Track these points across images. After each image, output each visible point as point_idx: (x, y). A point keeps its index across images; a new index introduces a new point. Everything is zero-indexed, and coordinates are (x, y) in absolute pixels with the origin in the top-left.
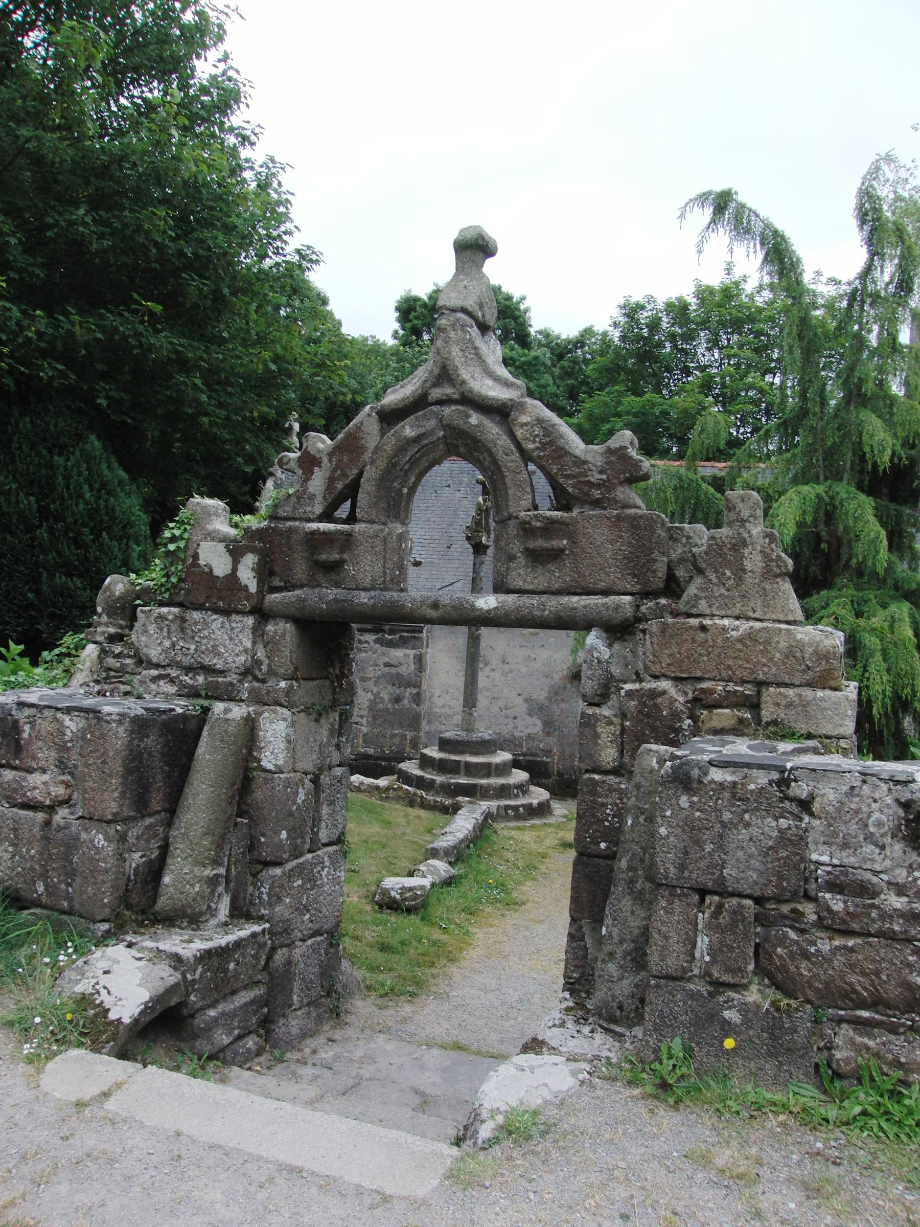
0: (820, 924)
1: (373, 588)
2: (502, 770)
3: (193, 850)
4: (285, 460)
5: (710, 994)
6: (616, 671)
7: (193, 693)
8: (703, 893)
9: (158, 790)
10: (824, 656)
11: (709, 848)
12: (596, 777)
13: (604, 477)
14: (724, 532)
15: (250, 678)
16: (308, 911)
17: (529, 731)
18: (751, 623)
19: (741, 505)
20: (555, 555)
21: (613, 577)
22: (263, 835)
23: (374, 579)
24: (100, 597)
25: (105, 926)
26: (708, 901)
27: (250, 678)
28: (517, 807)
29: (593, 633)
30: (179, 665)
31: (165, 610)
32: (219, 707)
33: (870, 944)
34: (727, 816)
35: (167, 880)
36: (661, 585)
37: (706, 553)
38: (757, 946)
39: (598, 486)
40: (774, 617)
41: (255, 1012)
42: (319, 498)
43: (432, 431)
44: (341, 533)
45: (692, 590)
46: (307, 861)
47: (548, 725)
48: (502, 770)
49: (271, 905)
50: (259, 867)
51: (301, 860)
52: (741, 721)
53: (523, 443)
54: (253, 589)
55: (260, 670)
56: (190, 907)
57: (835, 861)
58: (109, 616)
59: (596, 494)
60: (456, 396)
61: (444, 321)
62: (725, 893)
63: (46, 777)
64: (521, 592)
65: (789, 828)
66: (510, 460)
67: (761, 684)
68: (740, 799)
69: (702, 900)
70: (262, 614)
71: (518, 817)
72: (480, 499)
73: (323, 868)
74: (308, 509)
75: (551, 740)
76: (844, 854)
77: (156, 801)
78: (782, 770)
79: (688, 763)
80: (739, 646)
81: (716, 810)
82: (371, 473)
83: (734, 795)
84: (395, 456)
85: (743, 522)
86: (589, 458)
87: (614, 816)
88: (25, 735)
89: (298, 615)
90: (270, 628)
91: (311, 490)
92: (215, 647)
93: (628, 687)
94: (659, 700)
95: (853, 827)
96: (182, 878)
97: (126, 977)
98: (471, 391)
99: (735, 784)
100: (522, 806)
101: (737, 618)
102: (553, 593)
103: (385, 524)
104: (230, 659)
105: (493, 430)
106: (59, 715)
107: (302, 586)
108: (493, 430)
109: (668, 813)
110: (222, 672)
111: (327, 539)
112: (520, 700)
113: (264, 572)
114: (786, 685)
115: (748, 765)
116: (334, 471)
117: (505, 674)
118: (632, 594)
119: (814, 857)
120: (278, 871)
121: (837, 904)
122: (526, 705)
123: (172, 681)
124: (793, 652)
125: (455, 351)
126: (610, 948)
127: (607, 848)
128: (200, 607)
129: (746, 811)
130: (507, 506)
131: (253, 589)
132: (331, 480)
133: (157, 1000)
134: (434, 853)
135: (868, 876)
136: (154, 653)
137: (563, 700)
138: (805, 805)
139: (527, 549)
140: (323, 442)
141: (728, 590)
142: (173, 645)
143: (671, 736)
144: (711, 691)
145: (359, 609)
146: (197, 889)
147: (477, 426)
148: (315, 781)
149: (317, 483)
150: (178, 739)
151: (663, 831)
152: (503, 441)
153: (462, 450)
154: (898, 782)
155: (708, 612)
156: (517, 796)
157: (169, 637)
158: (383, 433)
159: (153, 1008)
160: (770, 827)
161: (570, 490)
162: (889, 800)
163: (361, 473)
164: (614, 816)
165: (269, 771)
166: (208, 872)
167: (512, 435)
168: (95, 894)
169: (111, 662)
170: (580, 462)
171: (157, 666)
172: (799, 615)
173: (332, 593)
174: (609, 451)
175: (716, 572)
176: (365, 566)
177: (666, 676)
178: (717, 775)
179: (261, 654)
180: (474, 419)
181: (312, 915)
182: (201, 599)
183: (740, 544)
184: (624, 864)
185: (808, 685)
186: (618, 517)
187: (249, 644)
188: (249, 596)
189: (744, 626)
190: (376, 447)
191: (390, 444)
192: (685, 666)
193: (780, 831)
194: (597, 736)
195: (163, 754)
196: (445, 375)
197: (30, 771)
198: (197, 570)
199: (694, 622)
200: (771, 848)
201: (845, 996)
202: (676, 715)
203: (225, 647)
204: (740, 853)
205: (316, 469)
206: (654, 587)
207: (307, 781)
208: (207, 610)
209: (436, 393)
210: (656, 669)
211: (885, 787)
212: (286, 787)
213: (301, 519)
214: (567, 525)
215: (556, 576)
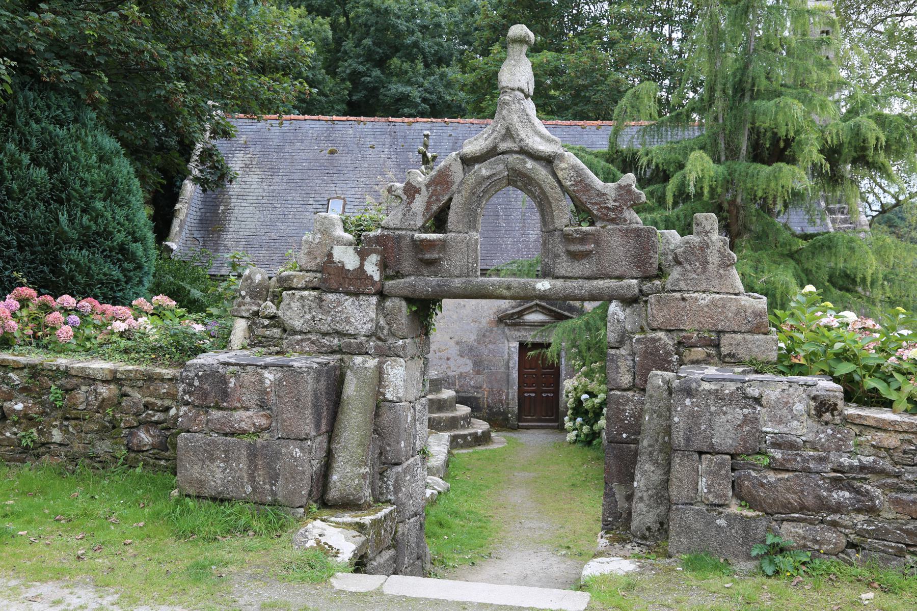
0: (769, 467)
3: (351, 457)
4: (393, 189)
5: (707, 510)
8: (701, 453)
10: (757, 314)
11: (703, 427)
12: (619, 393)
13: (617, 204)
14: (694, 239)
15: (374, 338)
18: (713, 295)
19: (705, 222)
20: (586, 255)
21: (624, 267)
22: (389, 445)
27: (374, 338)
31: (306, 293)
32: (359, 359)
34: (713, 409)
35: (335, 478)
37: (684, 252)
38: (733, 482)
39: (613, 210)
43: (500, 172)
44: (440, 240)
47: (479, 365)
52: (709, 355)
53: (563, 182)
54: (377, 277)
56: (353, 495)
57: (777, 431)
58: (251, 298)
59: (612, 215)
60: (517, 149)
61: (507, 98)
63: (250, 413)
64: (564, 277)
66: (554, 192)
67: (719, 332)
70: (382, 295)
74: (412, 223)
75: (480, 378)
80: (706, 309)
83: (716, 397)
85: (706, 233)
86: (607, 191)
88: (232, 385)
89: (410, 295)
90: (388, 304)
93: (637, 336)
95: (785, 411)
98: (527, 145)
99: (717, 390)
100: (470, 435)
101: (704, 292)
102: (589, 278)
103: (467, 233)
104: (359, 326)
105: (541, 173)
106: (259, 370)
107: (410, 275)
108: (541, 173)
110: (354, 336)
111: (431, 244)
112: (452, 342)
113: (384, 265)
114: (735, 332)
116: (430, 197)
118: (636, 278)
119: (764, 429)
121: (778, 455)
122: (458, 347)
124: (740, 312)
125: (515, 118)
126: (640, 494)
127: (627, 437)
128: (335, 291)
130: (553, 222)
131: (377, 277)
135: (795, 438)
136: (298, 324)
139: (567, 251)
142: (314, 317)
145: (455, 291)
146: (356, 482)
147: (532, 169)
149: (419, 204)
150: (335, 383)
152: (550, 179)
153: (519, 184)
154: (809, 386)
155: (685, 289)
157: (310, 312)
160: (738, 413)
161: (595, 212)
163: (450, 199)
164: (631, 417)
167: (554, 175)
168: (295, 489)
169: (260, 331)
170: (601, 194)
171: (301, 332)
172: (742, 288)
173: (433, 280)
174: (620, 187)
175: (690, 264)
177: (661, 330)
178: (706, 386)
179: (382, 322)
180: (530, 164)
183: (704, 247)
185: (749, 332)
186: (627, 230)
187: (374, 316)
188: (374, 283)
189: (709, 298)
190: (461, 182)
191: (471, 179)
192: (673, 322)
193: (744, 415)
195: (327, 393)
196: (509, 134)
197: (235, 409)
199: (677, 295)
200: (739, 425)
201: (784, 506)
202: (668, 353)
204: (722, 429)
205: (417, 195)
206: (651, 274)
208: (340, 292)
209: (503, 146)
210: (655, 325)
211: (802, 389)
214: (593, 235)
215: (584, 267)
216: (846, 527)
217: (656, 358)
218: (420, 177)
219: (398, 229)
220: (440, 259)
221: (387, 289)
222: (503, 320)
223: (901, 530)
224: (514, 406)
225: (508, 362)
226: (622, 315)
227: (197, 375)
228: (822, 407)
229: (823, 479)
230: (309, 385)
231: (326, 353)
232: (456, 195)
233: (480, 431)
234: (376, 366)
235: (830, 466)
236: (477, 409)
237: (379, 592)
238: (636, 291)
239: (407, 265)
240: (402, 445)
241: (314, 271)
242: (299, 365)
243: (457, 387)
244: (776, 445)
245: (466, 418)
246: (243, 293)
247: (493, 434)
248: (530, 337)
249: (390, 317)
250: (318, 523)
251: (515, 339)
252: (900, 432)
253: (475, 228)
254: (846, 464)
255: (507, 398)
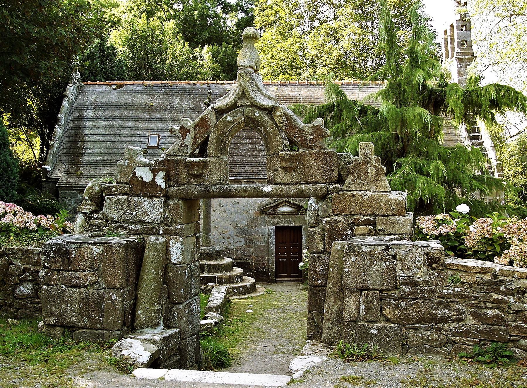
1: (216, 184)
2: (229, 267)
7: (136, 233)
8: (361, 290)
11: (363, 274)
12: (316, 255)
13: (312, 137)
15: (163, 225)
17: (237, 245)
21: (318, 176)
22: (174, 291)
26: (363, 293)
28: (239, 287)
31: (119, 197)
32: (153, 238)
36: (337, 179)
40: (380, 190)
44: (202, 162)
45: (349, 181)
47: (249, 242)
48: (229, 267)
54: (163, 187)
55: (168, 221)
62: (369, 290)
63: (85, 273)
67: (376, 216)
69: (361, 294)
70: (167, 197)
71: (241, 293)
75: (251, 249)
76: (408, 272)
78: (386, 245)
79: (354, 245)
83: (370, 255)
87: (323, 270)
91: (186, 143)
92: (146, 212)
94: (339, 224)
99: (370, 251)
100: (241, 286)
102: (296, 184)
103: (220, 157)
107: (184, 184)
109: (348, 264)
110: (150, 223)
112: (231, 227)
113: (167, 179)
115: (374, 245)
117: (221, 213)
120: (181, 306)
123: (124, 229)
124: (387, 203)
127: (321, 282)
128: (138, 195)
131: (163, 187)
132: (195, 139)
134: (211, 309)
135: (416, 279)
136: (115, 217)
137: (256, 226)
143: (343, 237)
144: (358, 219)
149: (189, 139)
152: (270, 122)
156: (237, 281)
158: (217, 119)
160: (382, 266)
163: (208, 136)
164: (323, 270)
165: (175, 264)
167: (273, 120)
170: (302, 131)
171: (117, 222)
178: (364, 249)
184: (330, 286)
186: (319, 153)
187: (162, 210)
188: (161, 190)
194: (315, 239)
203: (150, 212)
208: (141, 196)
209: (240, 103)
216: (446, 331)
217: (334, 233)
218: (190, 123)
219: (176, 156)
220: (203, 173)
221: (170, 193)
222: (264, 211)
223: (477, 331)
224: (272, 267)
225: (268, 239)
226: (315, 206)
227: (52, 250)
228: (431, 261)
229: (433, 303)
230: (119, 255)
231: (134, 234)
232: (212, 133)
233: (248, 284)
234: (163, 242)
235: (436, 295)
236: (248, 271)
237: (162, 379)
238: (324, 191)
239: (183, 177)
240: (182, 291)
241: (125, 183)
242: (114, 242)
243: (235, 256)
244: (406, 284)
245: (238, 276)
246: (86, 198)
247: (257, 286)
248: (285, 222)
249: (173, 210)
250: (129, 340)
251: (272, 224)
252: (476, 273)
253: (225, 154)
254: (446, 293)
255: (268, 262)
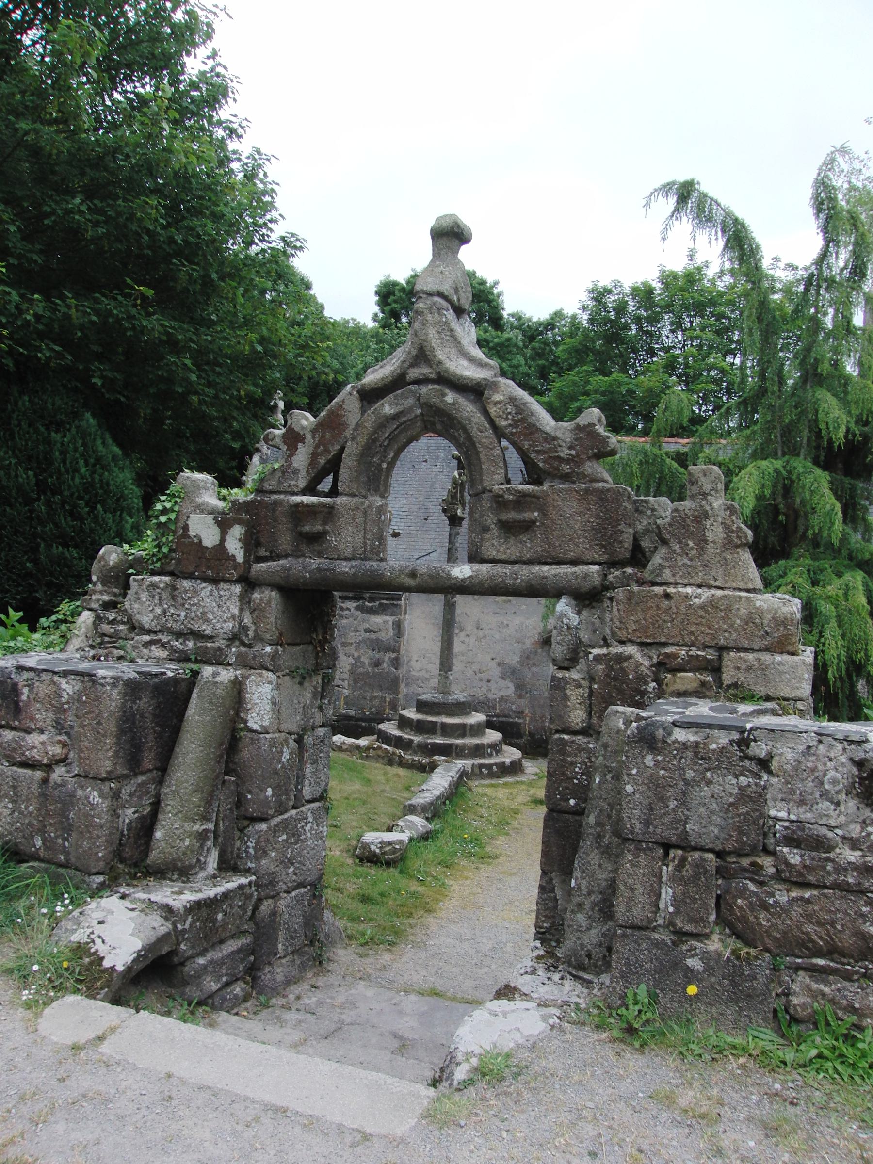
0: (778, 876)
1: (354, 558)
2: (477, 730)
3: (183, 806)
4: (270, 437)
5: (673, 943)
6: (585, 636)
7: (184, 658)
8: (667, 847)
9: (150, 749)
10: (782, 622)
11: (672, 804)
12: (566, 737)
13: (573, 452)
14: (687, 505)
15: (237, 643)
16: (292, 864)
17: (502, 693)
18: (713, 591)
19: (703, 479)
20: (527, 527)
21: (582, 547)
22: (250, 792)
23: (355, 550)
24: (95, 566)
25: (100, 879)
26: (671, 855)
27: (237, 643)
28: (491, 765)
29: (563, 600)
30: (170, 631)
31: (156, 579)
32: (207, 671)
33: (825, 896)
34: (690, 774)
35: (158, 834)
36: (627, 555)
37: (670, 525)
38: (718, 897)
39: (567, 461)
40: (735, 585)
41: (242, 960)
42: (303, 473)
43: (410, 409)
44: (324, 505)
45: (657, 559)
46: (291, 817)
47: (520, 687)
48: (477, 730)
49: (257, 859)
50: (246, 823)
51: (286, 816)
52: (703, 684)
53: (496, 420)
54: (240, 558)
55: (247, 636)
56: (181, 860)
57: (793, 817)
58: (103, 585)
59: (566, 468)
60: (433, 376)
61: (421, 305)
62: (688, 848)
63: (43, 737)
64: (494, 561)
65: (749, 786)
66: (484, 436)
67: (722, 649)
68: (702, 758)
69: (667, 854)
70: (249, 583)
71: (492, 775)
72: (456, 474)
73: (306, 824)
74: (293, 483)
75: (523, 702)
76: (801, 810)
77: (148, 760)
78: (742, 730)
79: (653, 724)
80: (702, 613)
81: (680, 769)
82: (352, 449)
83: (696, 754)
84: (375, 432)
85: (705, 495)
86: (559, 434)
87: (582, 774)
88: (24, 698)
89: (283, 583)
90: (256, 595)
91: (295, 465)
92: (204, 613)
93: (596, 651)
94: (626, 664)
95: (810, 785)
96: (173, 833)
97: (119, 927)
98: (447, 371)
99: (697, 743)
100: (496, 764)
101: (700, 586)
102: (525, 563)
103: (365, 497)
104: (218, 626)
105: (467, 408)
106: (56, 678)
107: (286, 556)
108: (467, 408)
109: (634, 771)
110: (210, 638)
111: (311, 511)
112: (493, 664)
113: (251, 542)
114: (746, 650)
115: (710, 726)
116: (317, 447)
117: (479, 639)
118: (599, 564)
119: (773, 813)
120: (264, 826)
121: (794, 857)
122: (499, 669)
123: (163, 646)
124: (753, 619)
125: (432, 333)
126: (579, 899)
127: (576, 804)
128: (190, 576)
129: (708, 770)
130: (481, 480)
131: (240, 558)
132: (314, 456)
133: (149, 949)
134: (412, 810)
135: (824, 831)
136: (146, 620)
137: (534, 664)
138: (764, 764)
139: (500, 521)
140: (307, 419)
141: (691, 560)
142: (165, 612)
143: (637, 698)
144: (675, 656)
145: (341, 577)
146: (187, 843)
147: (453, 404)
148: (299, 741)
149: (301, 458)
150: (169, 701)
151: (629, 788)
152: (478, 418)
153: (439, 427)
154: (852, 742)
155: (671, 580)
156: (490, 755)
157: (160, 605)
158: (363, 411)
159: (145, 957)
160: (730, 784)
161: (541, 465)
162: (843, 759)
163: (342, 449)
164: (582, 774)
165: (255, 732)
166: (198, 827)
167: (486, 413)
168: (90, 848)
169: (106, 628)
170: (550, 439)
171: (149, 632)
172: (759, 584)
173: (315, 563)
174: (578, 428)
175: (680, 542)
176: (346, 537)
177: (632, 642)
178: (680, 735)
179: (247, 620)
180: (450, 397)
181: (296, 868)
182: (191, 569)
183: (702, 516)
184: (592, 819)
185: (767, 649)
186: (587, 491)
187: (236, 611)
188: (236, 566)
189: (706, 594)
190: (357, 424)
191: (370, 421)
192: (650, 632)
193: (740, 788)
194: (566, 698)
195: (154, 715)
196: (422, 355)
197: (28, 731)
198: (187, 540)
199: (658, 590)
200: (731, 804)
201: (802, 944)
202: (641, 679)
203: (213, 613)
204: (702, 810)
205: (300, 445)
206: (621, 557)
207: (291, 741)
208: (196, 578)
209: (414, 373)
210: (622, 635)
211: (839, 747)
212: (271, 747)
213: (285, 493)
214: (538, 498)
215: (527, 546)
